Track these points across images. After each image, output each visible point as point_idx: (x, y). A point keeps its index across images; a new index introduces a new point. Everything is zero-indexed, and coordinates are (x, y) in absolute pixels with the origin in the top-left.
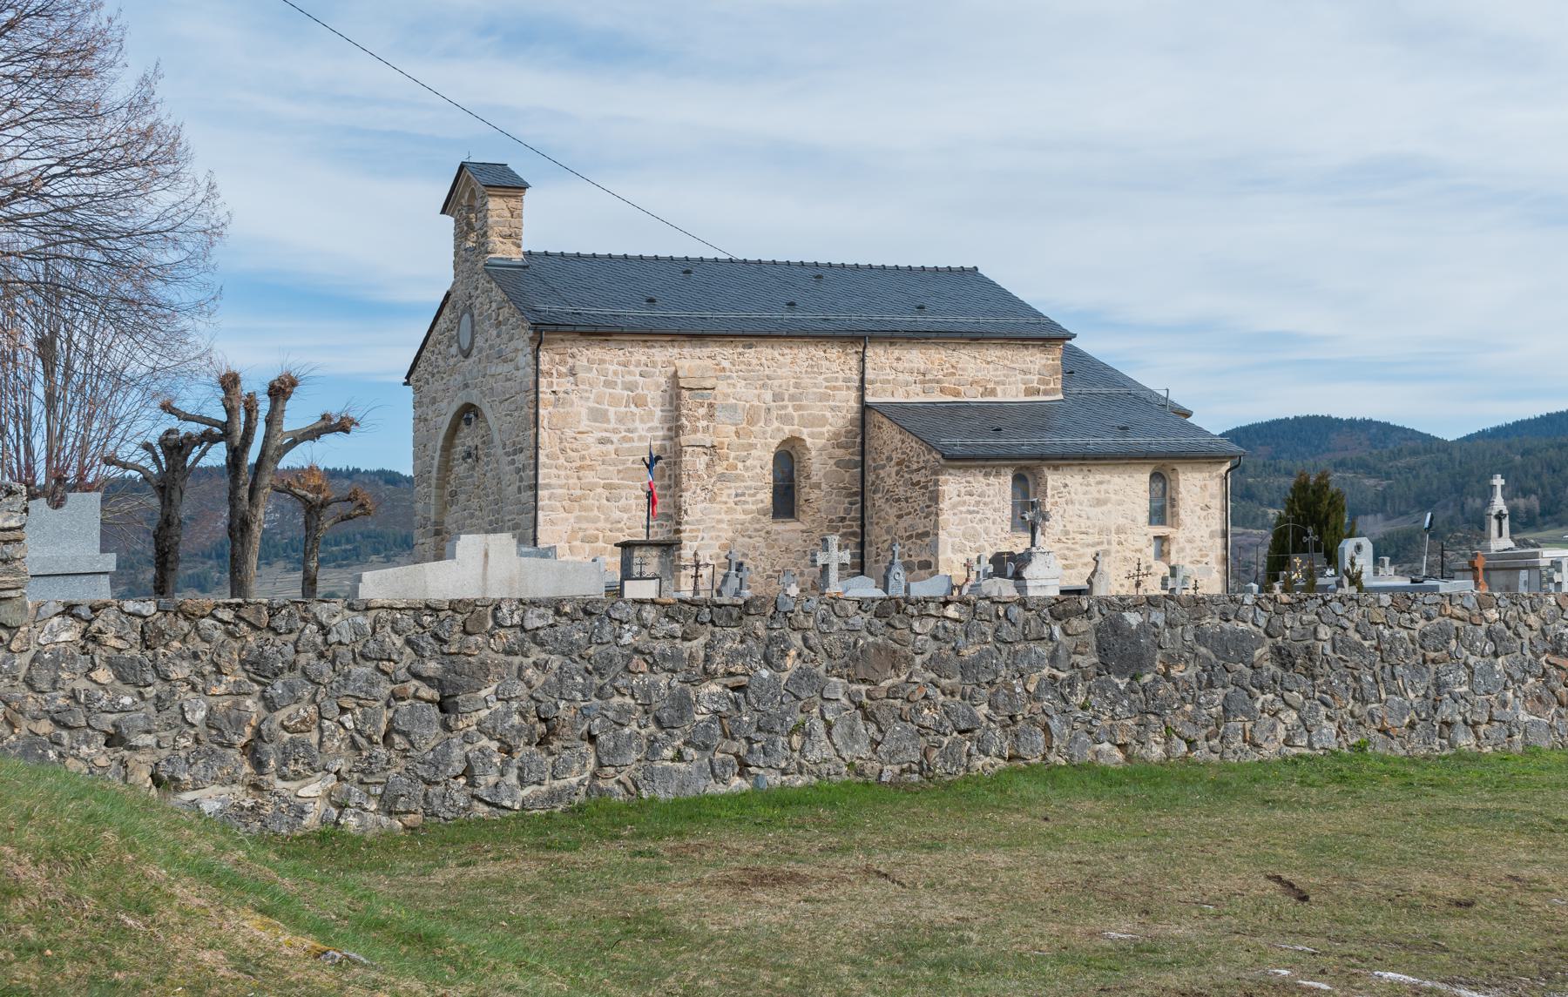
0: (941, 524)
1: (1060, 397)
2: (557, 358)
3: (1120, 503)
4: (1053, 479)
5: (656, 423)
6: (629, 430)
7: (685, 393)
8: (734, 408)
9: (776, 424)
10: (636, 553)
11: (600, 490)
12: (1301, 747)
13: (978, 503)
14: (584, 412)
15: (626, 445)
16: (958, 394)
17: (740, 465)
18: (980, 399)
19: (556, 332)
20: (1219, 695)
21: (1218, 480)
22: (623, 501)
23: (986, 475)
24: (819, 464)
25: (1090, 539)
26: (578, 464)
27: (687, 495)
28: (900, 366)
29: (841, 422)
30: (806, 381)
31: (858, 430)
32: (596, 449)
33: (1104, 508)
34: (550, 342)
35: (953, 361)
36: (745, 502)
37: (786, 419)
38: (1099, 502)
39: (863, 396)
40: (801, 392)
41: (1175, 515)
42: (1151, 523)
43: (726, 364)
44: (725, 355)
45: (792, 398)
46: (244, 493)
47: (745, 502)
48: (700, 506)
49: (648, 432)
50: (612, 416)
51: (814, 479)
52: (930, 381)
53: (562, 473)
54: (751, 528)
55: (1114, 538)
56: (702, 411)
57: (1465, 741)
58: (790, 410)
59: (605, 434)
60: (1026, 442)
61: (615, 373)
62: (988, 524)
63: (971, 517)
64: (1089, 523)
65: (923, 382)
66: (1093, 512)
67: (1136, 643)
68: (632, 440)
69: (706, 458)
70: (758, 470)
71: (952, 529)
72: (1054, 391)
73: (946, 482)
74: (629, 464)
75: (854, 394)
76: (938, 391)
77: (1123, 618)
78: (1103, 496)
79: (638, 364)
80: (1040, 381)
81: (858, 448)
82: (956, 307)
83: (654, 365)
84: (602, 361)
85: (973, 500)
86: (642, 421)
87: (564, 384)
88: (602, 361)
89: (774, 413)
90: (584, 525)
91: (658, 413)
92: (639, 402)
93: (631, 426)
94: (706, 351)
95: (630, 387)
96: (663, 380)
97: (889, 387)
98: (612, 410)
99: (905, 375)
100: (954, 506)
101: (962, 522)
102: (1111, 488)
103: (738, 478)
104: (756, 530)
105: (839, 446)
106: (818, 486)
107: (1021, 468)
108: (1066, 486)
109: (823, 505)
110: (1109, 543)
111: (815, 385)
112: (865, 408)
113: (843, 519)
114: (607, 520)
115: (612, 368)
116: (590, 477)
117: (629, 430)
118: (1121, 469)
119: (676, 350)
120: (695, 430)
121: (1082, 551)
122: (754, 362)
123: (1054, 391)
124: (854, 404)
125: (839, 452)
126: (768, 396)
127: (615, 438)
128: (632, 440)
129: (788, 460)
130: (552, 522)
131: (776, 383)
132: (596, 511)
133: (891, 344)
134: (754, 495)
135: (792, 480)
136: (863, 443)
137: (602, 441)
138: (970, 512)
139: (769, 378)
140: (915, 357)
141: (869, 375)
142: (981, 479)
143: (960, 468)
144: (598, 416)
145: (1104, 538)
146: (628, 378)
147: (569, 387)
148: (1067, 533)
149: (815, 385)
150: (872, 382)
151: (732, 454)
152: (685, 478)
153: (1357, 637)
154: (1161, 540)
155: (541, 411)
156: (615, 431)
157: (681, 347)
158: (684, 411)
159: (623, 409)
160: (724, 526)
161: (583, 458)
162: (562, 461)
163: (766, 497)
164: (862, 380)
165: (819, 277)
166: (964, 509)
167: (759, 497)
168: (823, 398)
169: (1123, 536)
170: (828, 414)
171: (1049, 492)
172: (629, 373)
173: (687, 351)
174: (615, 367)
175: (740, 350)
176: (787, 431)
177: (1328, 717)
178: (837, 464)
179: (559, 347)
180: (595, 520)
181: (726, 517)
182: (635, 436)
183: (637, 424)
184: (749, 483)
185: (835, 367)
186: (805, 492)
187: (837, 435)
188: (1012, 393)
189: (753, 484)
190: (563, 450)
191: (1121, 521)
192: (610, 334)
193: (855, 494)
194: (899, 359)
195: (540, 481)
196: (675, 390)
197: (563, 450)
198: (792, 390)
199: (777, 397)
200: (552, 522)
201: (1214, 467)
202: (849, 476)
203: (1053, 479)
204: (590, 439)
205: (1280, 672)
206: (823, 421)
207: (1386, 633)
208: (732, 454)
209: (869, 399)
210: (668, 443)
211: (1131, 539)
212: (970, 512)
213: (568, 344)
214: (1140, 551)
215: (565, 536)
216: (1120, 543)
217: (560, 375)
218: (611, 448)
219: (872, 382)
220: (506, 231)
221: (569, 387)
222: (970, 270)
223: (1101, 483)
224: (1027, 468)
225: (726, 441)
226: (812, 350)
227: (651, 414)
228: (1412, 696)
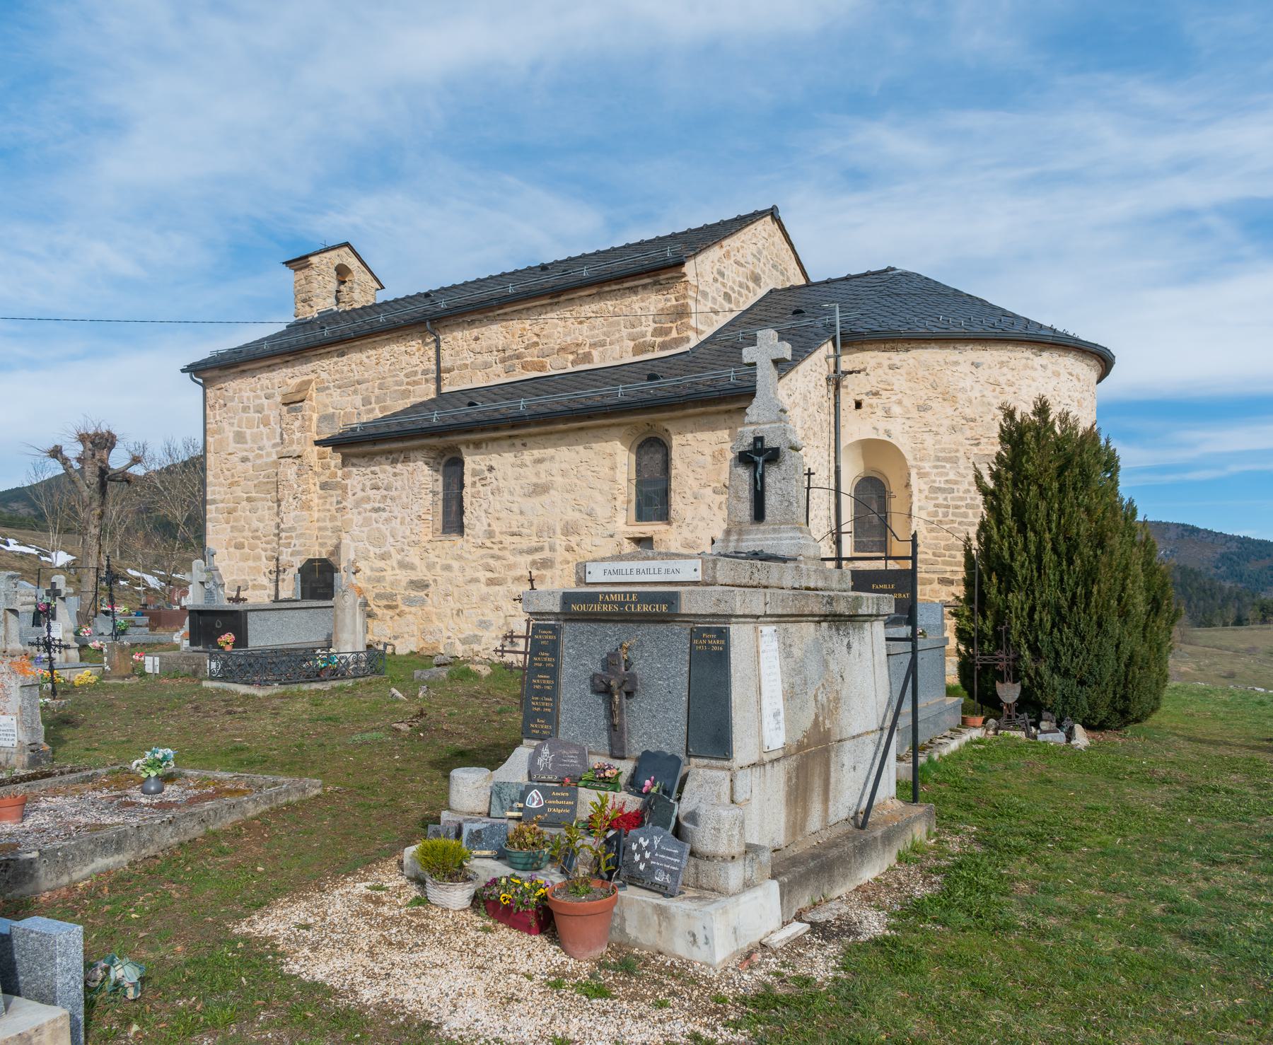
14: (231, 435)
18: (571, 369)
25: (524, 543)
32: (241, 467)
33: (545, 498)
38: (540, 489)
43: (324, 375)
50: (248, 437)
52: (510, 358)
55: (560, 541)
59: (245, 454)
61: (248, 399)
62: (395, 524)
65: (503, 361)
69: (295, 468)
71: (356, 531)
74: (261, 479)
75: (433, 387)
76: (518, 369)
78: (543, 479)
80: (658, 332)
92: (266, 423)
95: (259, 410)
97: (467, 372)
98: (248, 431)
101: (367, 522)
102: (555, 467)
108: (491, 469)
110: (552, 549)
117: (260, 448)
119: (290, 370)
121: (512, 559)
125: (180, 446)
126: (358, 400)
127: (251, 456)
128: (261, 456)
131: (364, 386)
137: (244, 460)
138: (377, 510)
140: (495, 334)
143: (363, 456)
144: (240, 438)
148: (490, 534)
150: (449, 371)
155: (208, 438)
159: (255, 430)
164: (439, 371)
166: (368, 507)
169: (574, 539)
175: (335, 359)
181: (328, 524)
182: (263, 453)
185: (415, 360)
191: (572, 515)
194: (477, 339)
195: (209, 497)
203: (473, 462)
204: (235, 459)
212: (377, 510)
218: (249, 464)
223: (540, 461)
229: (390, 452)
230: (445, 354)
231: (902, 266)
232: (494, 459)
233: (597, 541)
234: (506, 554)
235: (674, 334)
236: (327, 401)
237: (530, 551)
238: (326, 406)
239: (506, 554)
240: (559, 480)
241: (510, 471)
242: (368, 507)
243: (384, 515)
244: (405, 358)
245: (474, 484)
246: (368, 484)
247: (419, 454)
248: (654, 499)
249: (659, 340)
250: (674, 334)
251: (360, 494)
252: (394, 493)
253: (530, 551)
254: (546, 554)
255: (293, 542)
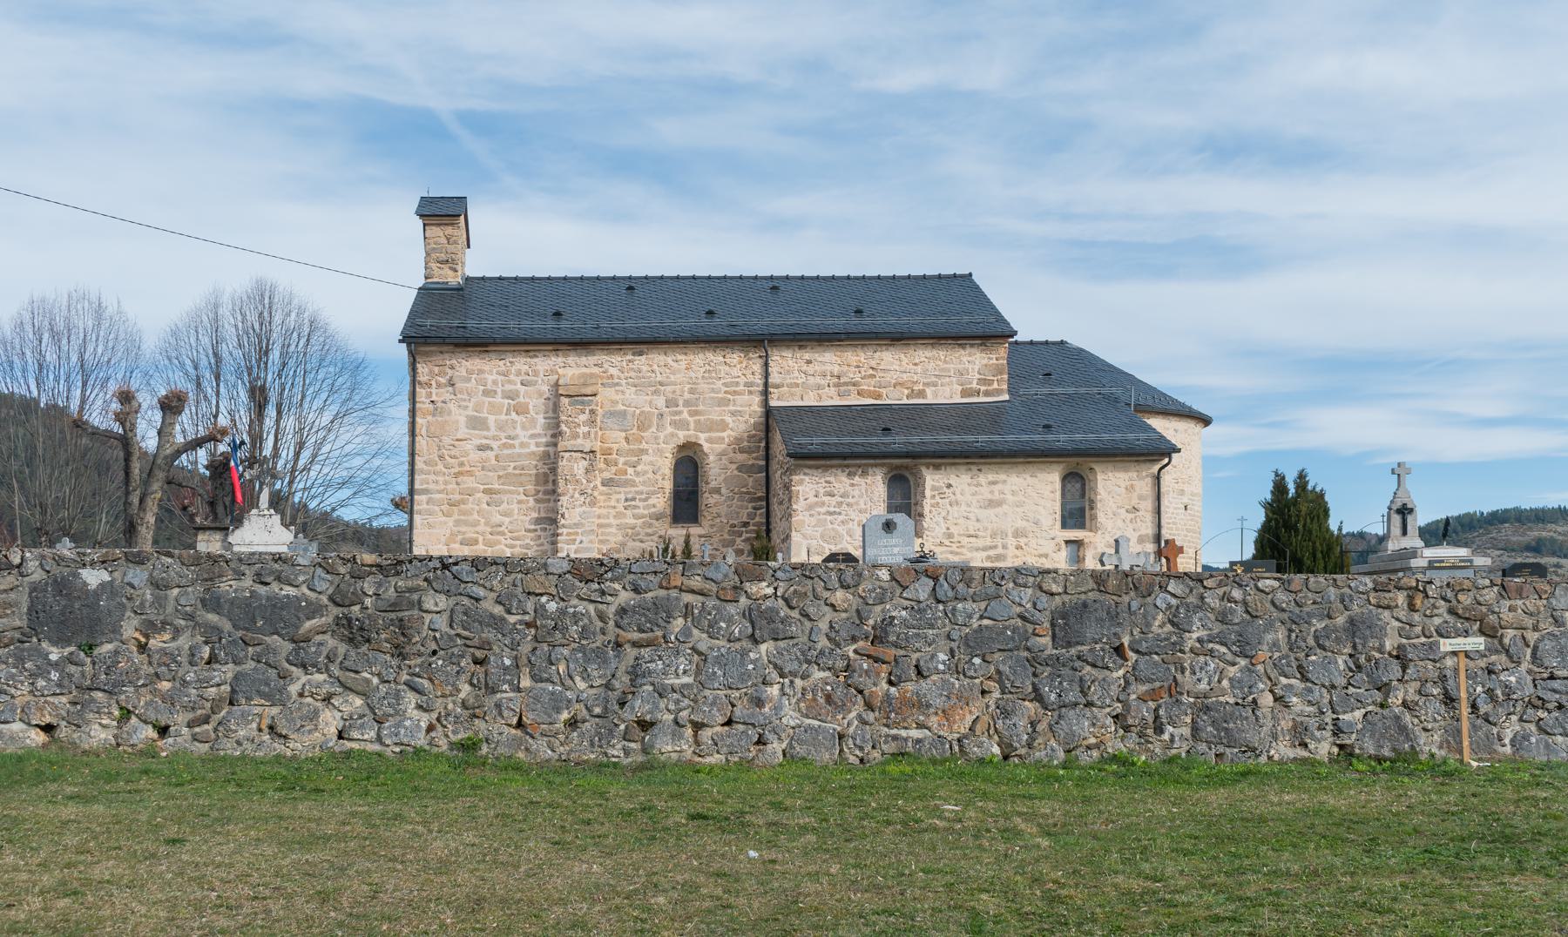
0: (794, 525)
1: (1006, 397)
2: (436, 370)
3: (1019, 505)
4: (932, 480)
5: (539, 430)
6: (509, 437)
7: (565, 401)
8: (623, 414)
9: (670, 429)
10: (200, 537)
11: (480, 495)
12: (364, 739)
13: (840, 504)
14: (462, 420)
15: (506, 452)
16: (879, 396)
17: (630, 470)
18: (905, 401)
19: (426, 344)
20: (228, 671)
21: (1149, 480)
22: (504, 506)
23: (850, 475)
24: (716, 471)
25: (980, 543)
26: (457, 470)
27: (564, 500)
28: (810, 369)
29: (743, 427)
30: (703, 386)
31: (762, 435)
32: (475, 456)
34: (427, 354)
35: (873, 363)
36: (636, 507)
37: (682, 425)
38: (992, 504)
39: (766, 400)
40: (713, 398)
41: (1094, 518)
42: (1064, 526)
43: (613, 371)
44: (613, 363)
45: (687, 403)
46: (135, 499)
47: (636, 507)
48: (578, 510)
49: (529, 439)
51: (713, 484)
52: (846, 384)
53: (441, 479)
54: (643, 532)
55: (1011, 542)
56: (583, 418)
57: (668, 747)
58: (685, 415)
59: (484, 441)
60: (898, 441)
63: (831, 514)
64: (978, 525)
65: (837, 385)
66: (983, 513)
67: (94, 606)
68: (513, 446)
69: (586, 463)
70: (650, 475)
72: (999, 392)
73: (801, 482)
74: (510, 470)
75: (757, 399)
76: (854, 394)
77: (76, 575)
78: (997, 496)
79: (519, 373)
80: (982, 381)
81: (762, 453)
82: (947, 311)
83: (536, 374)
84: (481, 372)
85: (833, 501)
86: (524, 428)
87: (446, 393)
88: (481, 372)
89: (668, 419)
90: (463, 529)
91: (541, 420)
92: (521, 410)
93: (512, 434)
94: (592, 359)
95: (511, 396)
96: (545, 388)
99: (812, 379)
100: (810, 507)
101: (820, 523)
102: (1007, 488)
103: (632, 483)
104: (648, 535)
105: (742, 451)
106: (717, 491)
107: (897, 467)
108: (949, 486)
109: (723, 510)
110: (1004, 547)
111: (713, 390)
112: (768, 412)
113: (746, 524)
114: (487, 524)
115: (490, 378)
116: (469, 482)
117: (509, 437)
118: (1021, 468)
120: (575, 436)
122: (645, 368)
123: (999, 392)
124: (755, 405)
125: (741, 457)
126: (660, 402)
127: (495, 445)
128: (513, 446)
129: (688, 465)
130: (430, 526)
131: (669, 388)
132: (476, 516)
133: (800, 347)
134: (646, 500)
135: (696, 484)
136: (767, 448)
137: (482, 448)
138: (831, 514)
139: (661, 384)
140: (829, 360)
141: (774, 378)
142: (844, 479)
143: (817, 467)
144: (477, 423)
145: (999, 542)
146: (508, 387)
147: (448, 397)
148: (950, 536)
149: (713, 390)
151: (622, 460)
152: (561, 483)
153: (498, 610)
154: (1077, 544)
155: (419, 420)
156: (495, 438)
157: (566, 356)
158: (563, 418)
159: (503, 417)
160: (613, 530)
161: (462, 464)
162: (440, 467)
163: (661, 501)
164: (766, 385)
165: (774, 288)
166: (823, 510)
167: (651, 502)
168: (723, 402)
169: (1023, 541)
170: (729, 419)
171: (928, 493)
172: (510, 382)
173: (572, 359)
174: (494, 377)
176: (682, 436)
177: (419, 707)
178: (739, 469)
179: (438, 359)
180: (475, 524)
182: (516, 442)
183: (519, 431)
184: (641, 488)
185: (735, 372)
186: (708, 499)
187: (738, 440)
188: (946, 393)
189: (645, 489)
190: (441, 457)
191: (1020, 524)
192: (486, 345)
193: (760, 499)
194: (809, 362)
196: (556, 394)
197: (441, 457)
198: (687, 396)
199: (670, 403)
200: (430, 526)
201: (1143, 466)
202: (753, 482)
203: (932, 480)
204: (468, 446)
205: (342, 648)
206: (723, 426)
207: (552, 606)
208: (622, 460)
209: (773, 403)
210: (551, 449)
211: (1034, 541)
212: (831, 514)
213: (446, 356)
214: (1046, 556)
215: (443, 539)
216: (1019, 547)
217: (439, 385)
218: (491, 454)
219: (777, 387)
220: (443, 257)
221: (448, 397)
222: (962, 276)
223: (994, 483)
224: (907, 468)
225: (615, 447)
226: (710, 355)
227: (533, 421)
228: (581, 685)
229: (847, 466)
230: (773, 369)
231: (1075, 340)
232: (953, 480)
233: (1041, 542)
234: (964, 551)
235: (995, 386)
236: (617, 397)
237: (985, 549)
238: (615, 402)
239: (964, 551)
240: (1009, 497)
241: (967, 488)
242: (823, 510)
243: (841, 518)
244: (724, 368)
245: (933, 497)
246: (822, 491)
247: (878, 471)
248: (1077, 514)
249: (983, 388)
250: (995, 386)
251: (812, 500)
252: (850, 500)
253: (985, 549)
254: (1000, 551)
255: (579, 539)
